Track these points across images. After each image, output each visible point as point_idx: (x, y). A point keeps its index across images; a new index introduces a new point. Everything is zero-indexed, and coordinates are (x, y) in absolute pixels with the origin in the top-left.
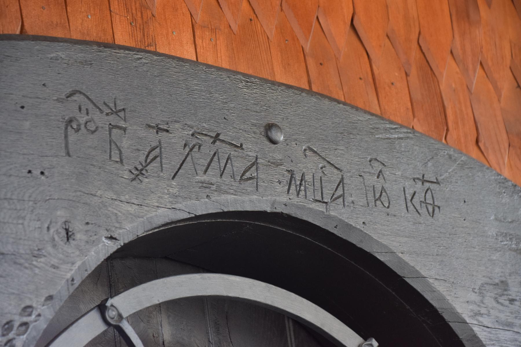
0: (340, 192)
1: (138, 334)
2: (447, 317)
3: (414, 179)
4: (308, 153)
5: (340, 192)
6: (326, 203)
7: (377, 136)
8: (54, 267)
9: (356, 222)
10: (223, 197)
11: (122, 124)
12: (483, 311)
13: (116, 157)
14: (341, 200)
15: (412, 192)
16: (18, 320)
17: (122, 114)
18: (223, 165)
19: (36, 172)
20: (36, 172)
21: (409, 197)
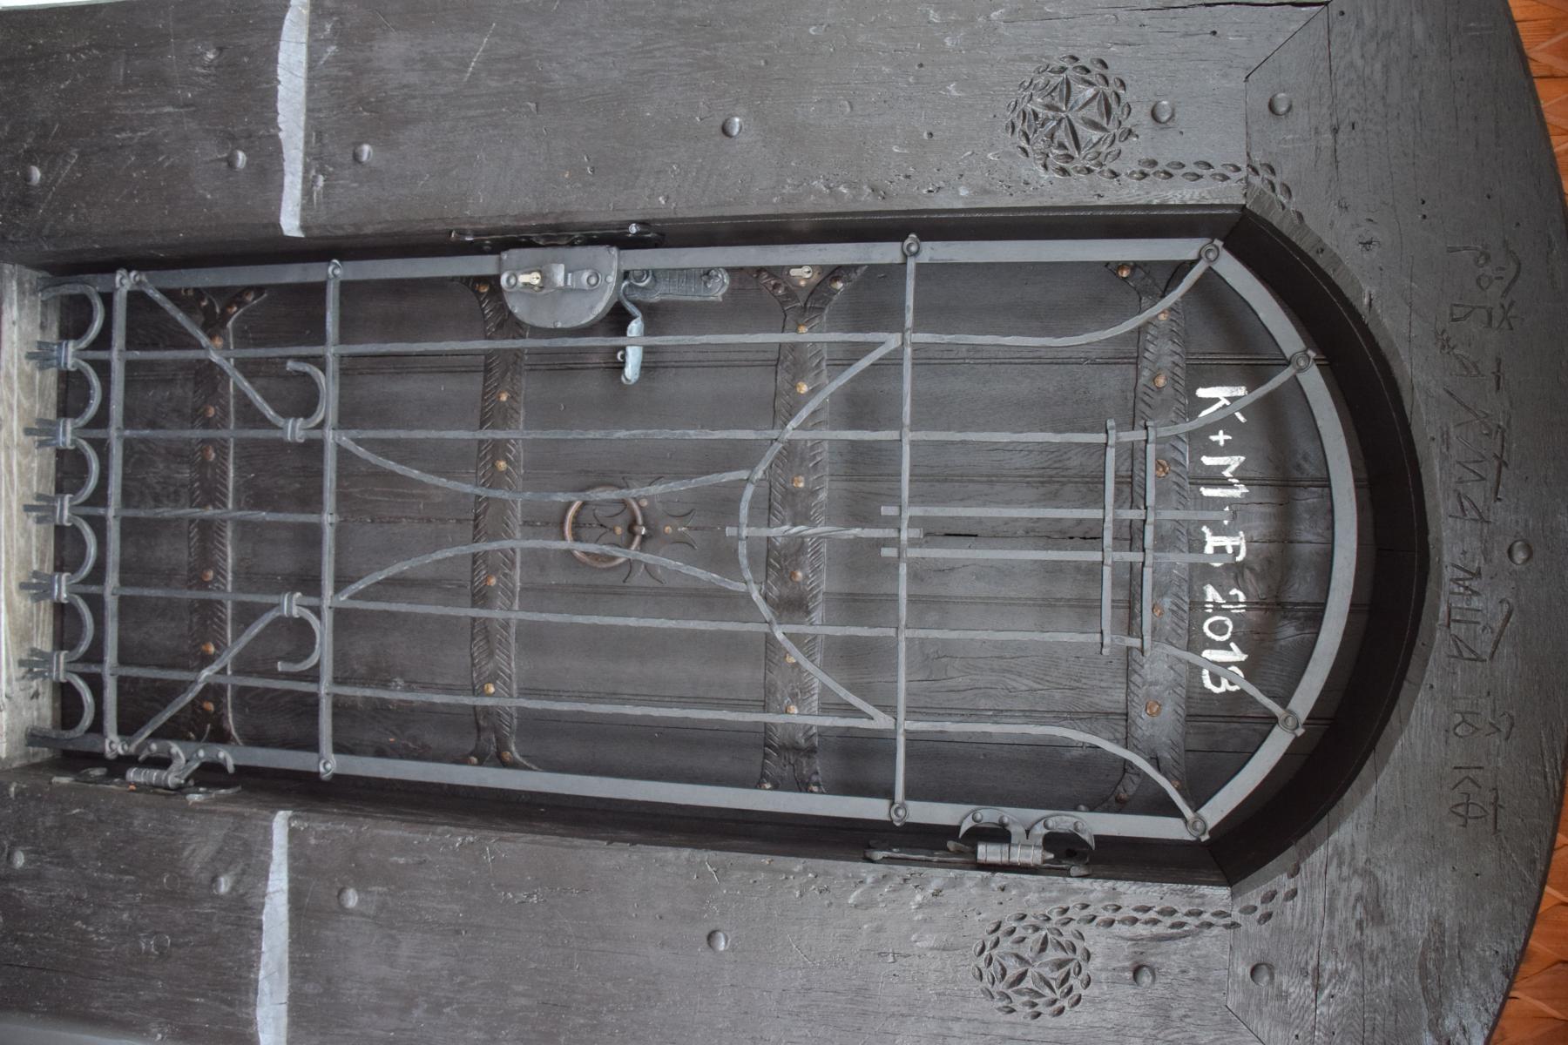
0: (1466, 654)
1: (829, 792)
2: (1333, 812)
3: (1495, 789)
4: (1505, 607)
5: (1466, 654)
6: (1449, 626)
7: (1207, 461)
8: (1332, 224)
9: (1432, 675)
10: (1436, 463)
11: (1495, 324)
12: (1345, 871)
13: (1458, 312)
14: (1455, 653)
15: (1480, 781)
16: (1276, 180)
17: (1505, 325)
18: (1471, 466)
19: (1424, 210)
20: (1424, 210)
21: (1472, 773)
